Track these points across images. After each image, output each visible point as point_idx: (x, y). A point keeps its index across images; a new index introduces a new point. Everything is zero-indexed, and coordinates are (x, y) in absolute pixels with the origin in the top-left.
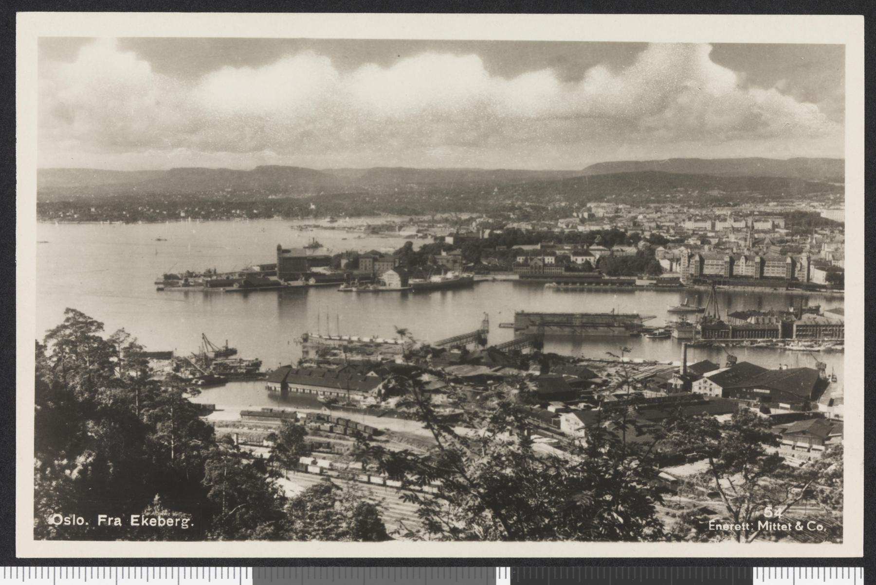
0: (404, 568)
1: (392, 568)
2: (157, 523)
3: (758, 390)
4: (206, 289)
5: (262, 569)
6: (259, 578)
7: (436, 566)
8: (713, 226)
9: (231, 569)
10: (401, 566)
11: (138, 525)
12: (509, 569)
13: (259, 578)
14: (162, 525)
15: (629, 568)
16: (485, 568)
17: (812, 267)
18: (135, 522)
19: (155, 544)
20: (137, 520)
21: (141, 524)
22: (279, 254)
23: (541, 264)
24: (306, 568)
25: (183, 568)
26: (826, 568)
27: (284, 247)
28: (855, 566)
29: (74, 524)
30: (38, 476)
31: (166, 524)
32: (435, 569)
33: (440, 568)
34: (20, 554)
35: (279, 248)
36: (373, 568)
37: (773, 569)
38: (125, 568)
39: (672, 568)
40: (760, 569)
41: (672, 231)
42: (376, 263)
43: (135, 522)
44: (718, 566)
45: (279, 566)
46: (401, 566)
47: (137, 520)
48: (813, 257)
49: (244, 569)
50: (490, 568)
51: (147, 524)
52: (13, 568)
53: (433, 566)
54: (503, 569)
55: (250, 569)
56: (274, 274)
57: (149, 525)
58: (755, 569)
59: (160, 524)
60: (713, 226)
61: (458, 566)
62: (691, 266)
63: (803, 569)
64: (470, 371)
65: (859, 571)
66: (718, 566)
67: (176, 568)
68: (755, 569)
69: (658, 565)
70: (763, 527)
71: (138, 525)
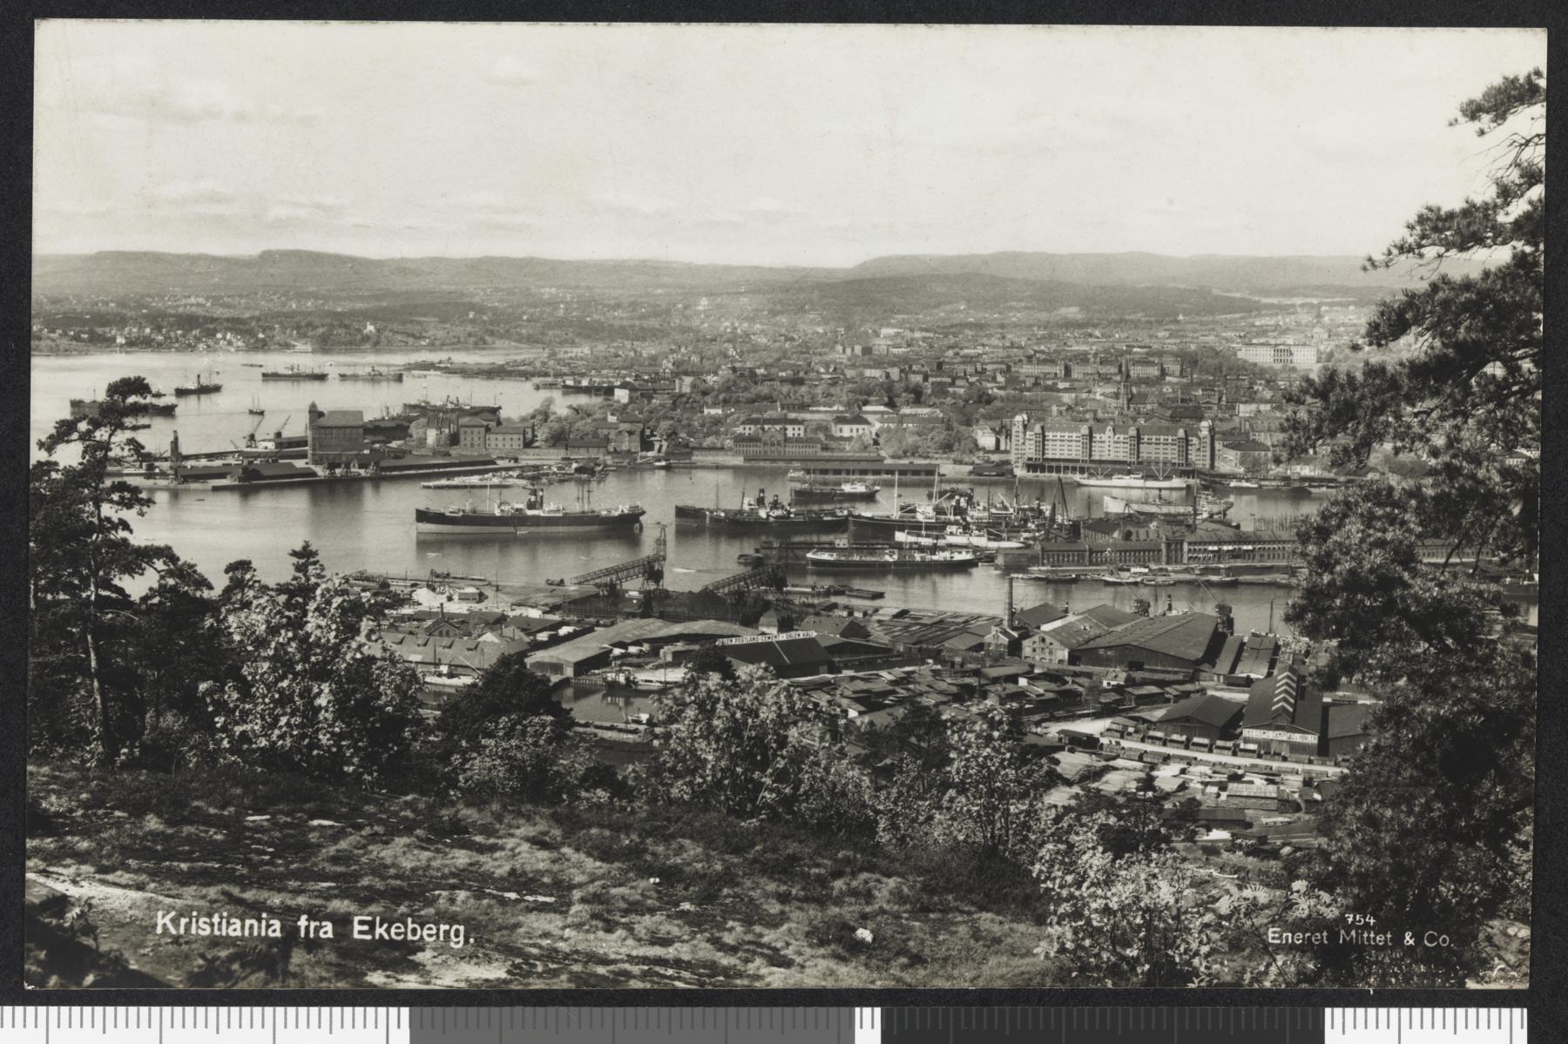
2: (405, 934)
3: (906, 1023)
4: (172, 485)
5: (427, 1010)
7: (745, 1005)
8: (1068, 371)
11: (369, 937)
12: (878, 1010)
13: (421, 1027)
14: (416, 938)
15: (1097, 1008)
16: (835, 1009)
17: (1218, 445)
18: (361, 932)
20: (366, 928)
21: (374, 935)
22: (312, 421)
23: (780, 437)
27: (321, 408)
28: (1511, 1006)
29: (255, 934)
31: (422, 937)
33: (752, 1009)
35: (500, 408)
38: (62, 1008)
40: (1338, 1011)
41: (1000, 379)
42: (492, 437)
44: (1261, 1006)
45: (458, 1005)
46: (681, 1005)
47: (366, 928)
48: (1221, 426)
50: (844, 1010)
51: (386, 937)
53: (727, 1005)
54: (867, 1011)
55: (405, 1011)
56: (303, 456)
57: (391, 939)
58: (1328, 1011)
59: (410, 937)
60: (1068, 371)
61: (786, 1005)
62: (1027, 442)
64: (660, 628)
65: (1519, 1015)
66: (1261, 1006)
68: (1328, 1011)
71: (369, 937)
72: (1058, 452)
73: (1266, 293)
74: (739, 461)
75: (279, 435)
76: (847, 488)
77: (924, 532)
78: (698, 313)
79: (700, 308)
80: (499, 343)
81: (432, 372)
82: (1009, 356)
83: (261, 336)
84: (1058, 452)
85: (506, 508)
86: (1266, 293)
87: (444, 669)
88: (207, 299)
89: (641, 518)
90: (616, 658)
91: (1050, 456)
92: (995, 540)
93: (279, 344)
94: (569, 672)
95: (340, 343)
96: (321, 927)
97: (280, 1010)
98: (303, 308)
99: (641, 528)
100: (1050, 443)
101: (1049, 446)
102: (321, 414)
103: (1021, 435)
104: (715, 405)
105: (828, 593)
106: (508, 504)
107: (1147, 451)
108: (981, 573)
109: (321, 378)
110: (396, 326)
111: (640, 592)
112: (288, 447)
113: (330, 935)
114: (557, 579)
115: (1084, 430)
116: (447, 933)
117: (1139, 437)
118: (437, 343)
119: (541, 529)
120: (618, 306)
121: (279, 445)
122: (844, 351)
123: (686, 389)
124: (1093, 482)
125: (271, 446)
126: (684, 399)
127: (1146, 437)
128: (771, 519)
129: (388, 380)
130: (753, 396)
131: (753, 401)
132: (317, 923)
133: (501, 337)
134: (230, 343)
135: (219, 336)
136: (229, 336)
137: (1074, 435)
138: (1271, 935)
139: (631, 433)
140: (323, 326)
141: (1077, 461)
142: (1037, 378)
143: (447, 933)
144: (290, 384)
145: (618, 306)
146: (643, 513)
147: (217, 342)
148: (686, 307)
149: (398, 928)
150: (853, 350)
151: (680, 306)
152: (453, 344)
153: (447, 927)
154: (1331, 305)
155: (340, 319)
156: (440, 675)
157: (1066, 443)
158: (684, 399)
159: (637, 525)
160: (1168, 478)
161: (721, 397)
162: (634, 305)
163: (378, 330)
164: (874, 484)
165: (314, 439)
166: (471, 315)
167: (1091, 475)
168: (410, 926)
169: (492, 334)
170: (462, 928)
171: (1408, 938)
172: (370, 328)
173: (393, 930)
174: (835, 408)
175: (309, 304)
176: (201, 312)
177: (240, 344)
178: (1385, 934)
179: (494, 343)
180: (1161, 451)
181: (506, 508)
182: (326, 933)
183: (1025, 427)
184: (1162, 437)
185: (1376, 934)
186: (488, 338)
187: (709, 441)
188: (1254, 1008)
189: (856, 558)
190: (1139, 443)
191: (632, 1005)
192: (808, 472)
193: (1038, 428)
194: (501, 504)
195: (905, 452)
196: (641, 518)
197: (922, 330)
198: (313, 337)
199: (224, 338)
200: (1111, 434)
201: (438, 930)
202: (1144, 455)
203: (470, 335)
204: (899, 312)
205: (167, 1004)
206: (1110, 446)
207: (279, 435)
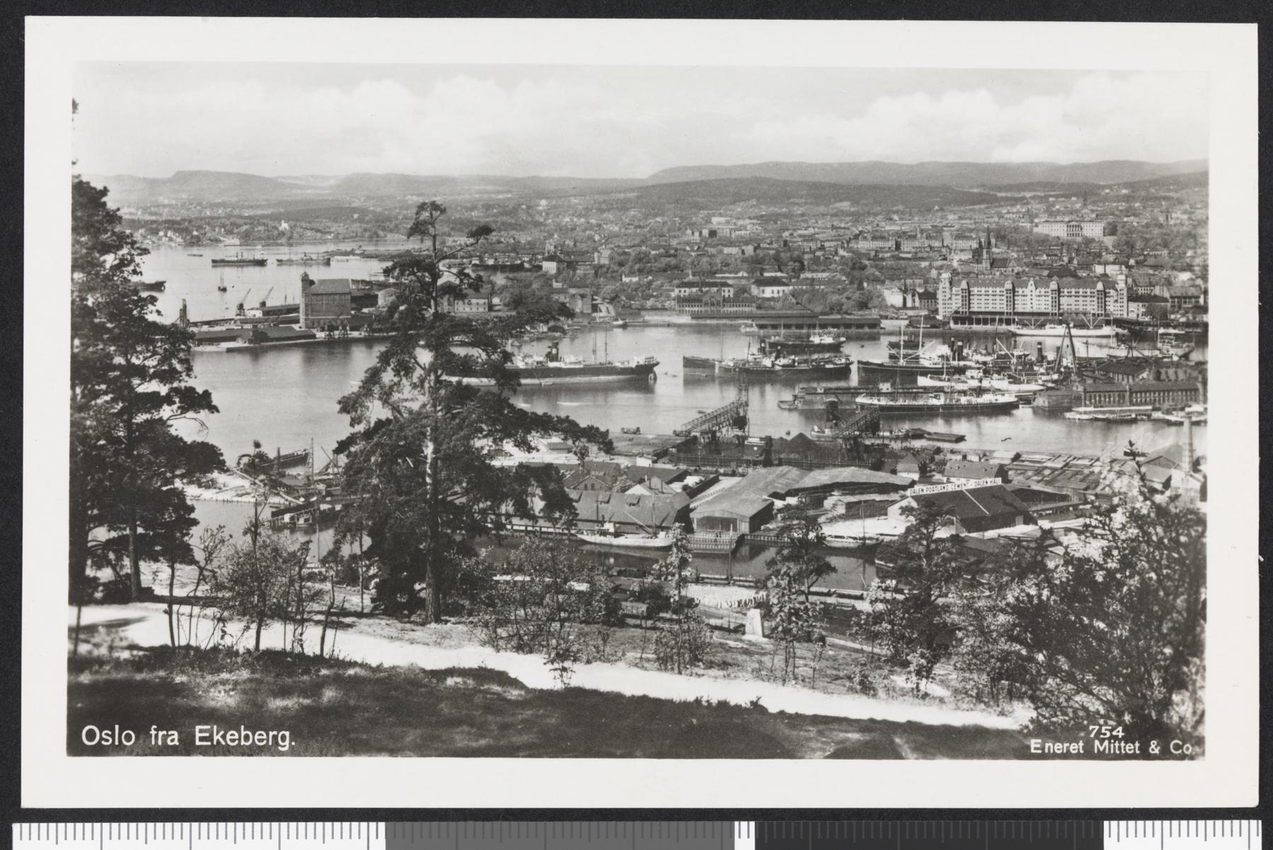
0: (603, 824)
1: (585, 824)
2: (239, 739)
5: (399, 825)
6: (395, 837)
8: (898, 246)
9: (1140, 823)
10: (599, 820)
12: (752, 824)
14: (248, 744)
18: (202, 739)
19: (654, 693)
22: (304, 289)
24: (461, 824)
25: (286, 823)
26: (1200, 822)
28: (341, 820)
30: (78, 390)
32: (647, 824)
34: (28, 801)
36: (558, 824)
37: (1131, 823)
38: (202, 824)
39: (987, 822)
40: (1114, 823)
43: (202, 739)
44: (1054, 819)
45: (423, 820)
49: (373, 825)
50: (726, 823)
51: (223, 743)
52: (371, 823)
54: (744, 824)
55: (382, 825)
58: (1106, 823)
59: (243, 743)
61: (680, 820)
62: (954, 297)
63: (1175, 823)
65: (1255, 826)
66: (1054, 819)
67: (275, 825)
68: (1106, 823)
69: (968, 819)
70: (1101, 749)
72: (983, 306)
73: (1000, 189)
74: (685, 319)
75: (263, 304)
76: (816, 340)
77: (944, 376)
78: (540, 213)
79: (541, 208)
80: (389, 236)
81: (351, 257)
82: (839, 236)
83: (195, 233)
84: (983, 306)
85: (529, 361)
86: (1000, 189)
87: (609, 527)
88: (137, 209)
89: (655, 369)
90: (780, 511)
91: (975, 309)
92: (1014, 383)
93: (210, 240)
94: (744, 528)
95: (260, 239)
96: (168, 736)
97: (151, 825)
98: (216, 215)
99: (655, 379)
100: (976, 297)
101: (975, 300)
102: (312, 283)
103: (948, 290)
104: (631, 273)
105: (906, 437)
106: (531, 356)
107: (1067, 303)
108: (1024, 412)
109: (262, 263)
110: (304, 225)
111: (761, 439)
112: (283, 314)
113: (176, 742)
114: (634, 427)
115: (1008, 286)
116: (275, 737)
117: (1059, 291)
118: (341, 236)
119: (568, 380)
120: (473, 208)
121: (267, 313)
122: (693, 233)
123: (605, 261)
124: (1025, 331)
125: (259, 314)
126: (605, 269)
127: (1066, 290)
128: (778, 368)
129: (318, 264)
130: (663, 265)
131: (665, 270)
132: (165, 732)
133: (391, 231)
134: (171, 239)
135: (161, 234)
136: (170, 233)
137: (998, 290)
138: (1033, 746)
139: (583, 296)
140: (245, 224)
141: (1002, 313)
142: (876, 251)
143: (275, 737)
144: (235, 269)
145: (473, 208)
146: (657, 364)
147: (160, 239)
148: (529, 207)
149: (232, 735)
150: (701, 233)
151: (524, 207)
152: (352, 237)
153: (275, 733)
154: (1057, 196)
155: (254, 220)
156: (604, 533)
157: (990, 297)
158: (605, 269)
159: (652, 375)
160: (1099, 327)
161: (637, 267)
162: (488, 207)
163: (291, 227)
164: (838, 336)
165: (306, 306)
166: (356, 216)
167: (1025, 325)
168: (243, 733)
169: (384, 229)
170: (287, 734)
171: (1153, 746)
172: (284, 226)
173: (228, 737)
174: (740, 274)
175: (220, 211)
176: (135, 218)
177: (179, 240)
178: (1134, 744)
179: (386, 236)
180: (1081, 303)
181: (529, 361)
182: (172, 740)
183: (951, 283)
184: (1081, 290)
185: (1126, 743)
186: (381, 233)
187: (649, 303)
188: (1048, 822)
189: (900, 402)
190: (1059, 296)
191: (559, 820)
192: (761, 327)
193: (964, 285)
194: (525, 357)
195: (832, 309)
196: (655, 369)
197: (750, 218)
198: (238, 234)
199: (166, 236)
200: (1033, 287)
201: (268, 735)
202: (1065, 307)
203: (365, 230)
204: (703, 209)
205: (195, 821)
206: (1033, 299)
207: (263, 304)
